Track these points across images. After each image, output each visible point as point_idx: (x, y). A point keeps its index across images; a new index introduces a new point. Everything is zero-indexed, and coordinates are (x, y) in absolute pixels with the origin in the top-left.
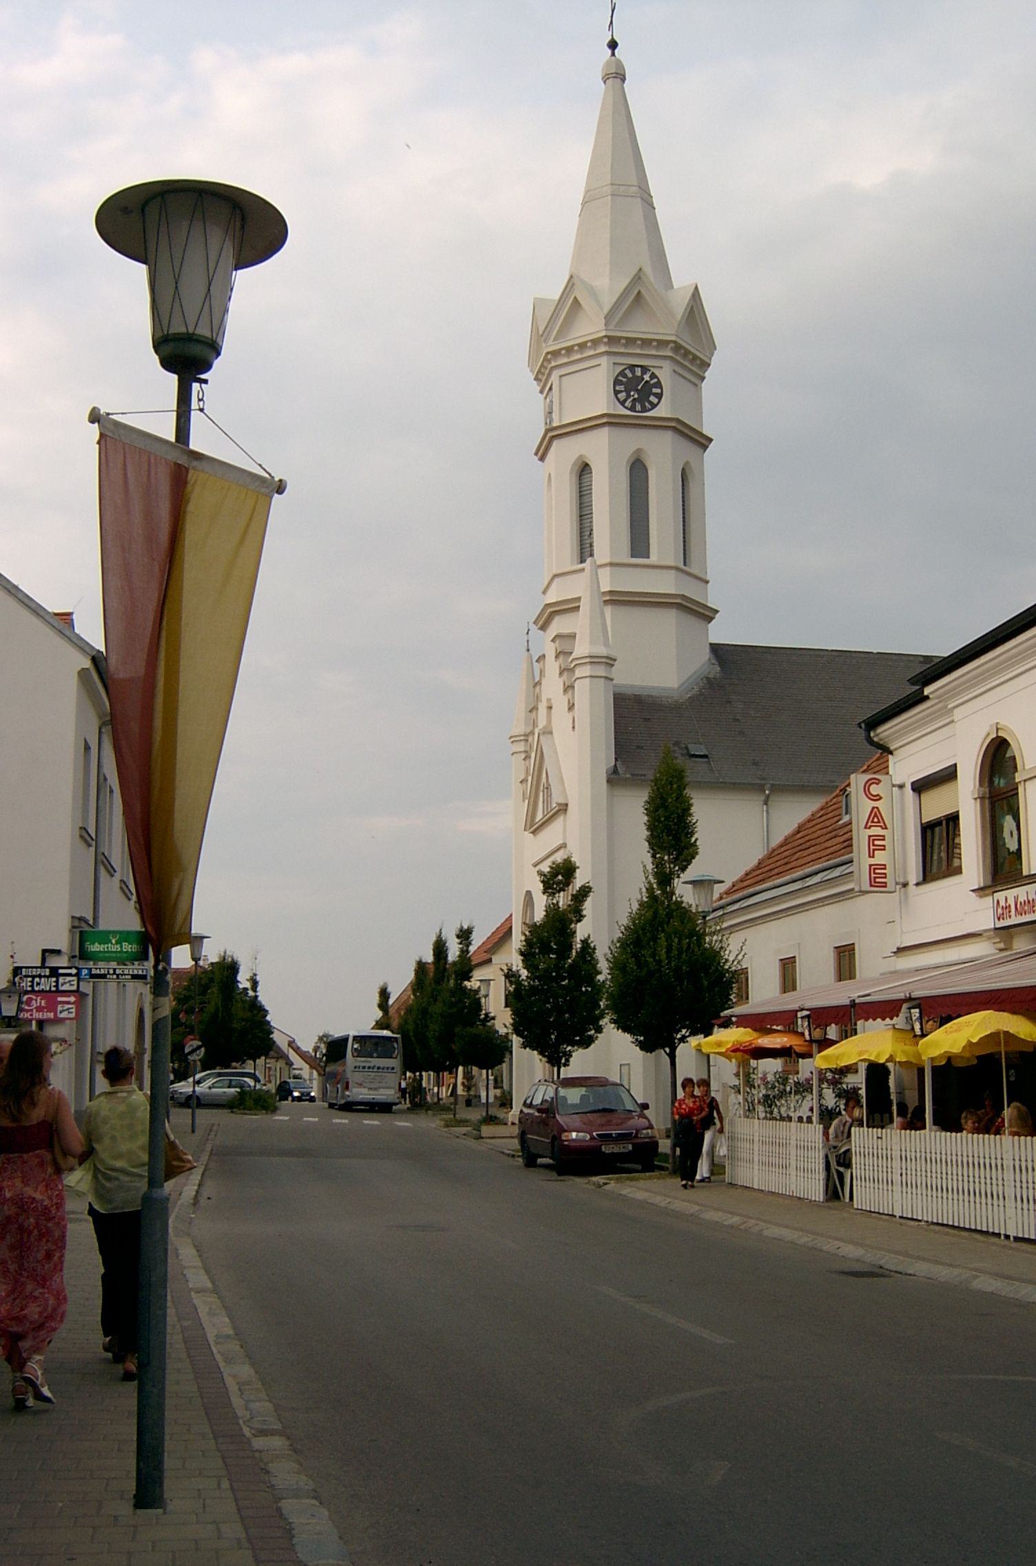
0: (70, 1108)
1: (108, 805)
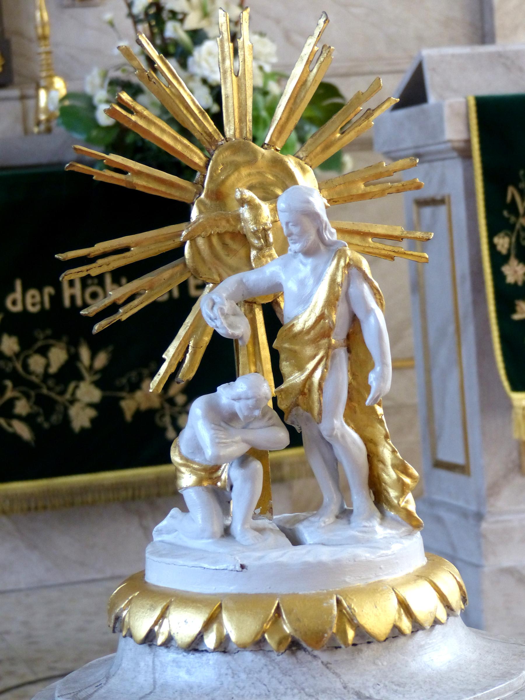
0: (289, 516)
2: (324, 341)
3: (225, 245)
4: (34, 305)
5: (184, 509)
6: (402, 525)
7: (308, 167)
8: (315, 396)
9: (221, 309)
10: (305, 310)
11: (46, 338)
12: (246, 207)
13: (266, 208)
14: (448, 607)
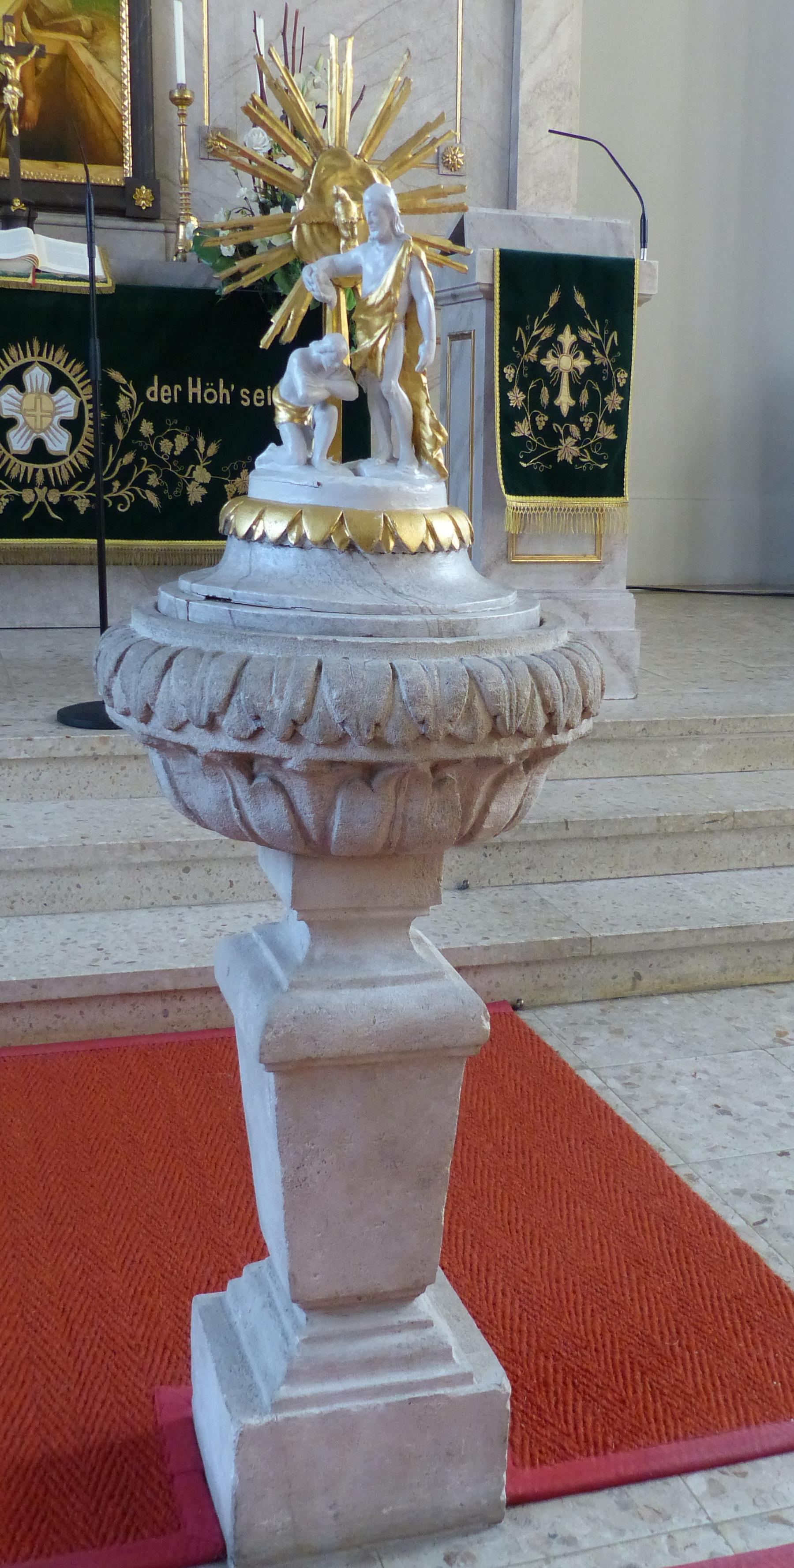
1: (440, 1391)
2: (389, 315)
3: (322, 234)
4: (166, 398)
5: (279, 442)
6: (433, 473)
7: (387, 180)
8: (380, 359)
9: (317, 276)
10: (377, 287)
11: (174, 426)
12: (339, 202)
13: (354, 207)
14: (461, 538)
